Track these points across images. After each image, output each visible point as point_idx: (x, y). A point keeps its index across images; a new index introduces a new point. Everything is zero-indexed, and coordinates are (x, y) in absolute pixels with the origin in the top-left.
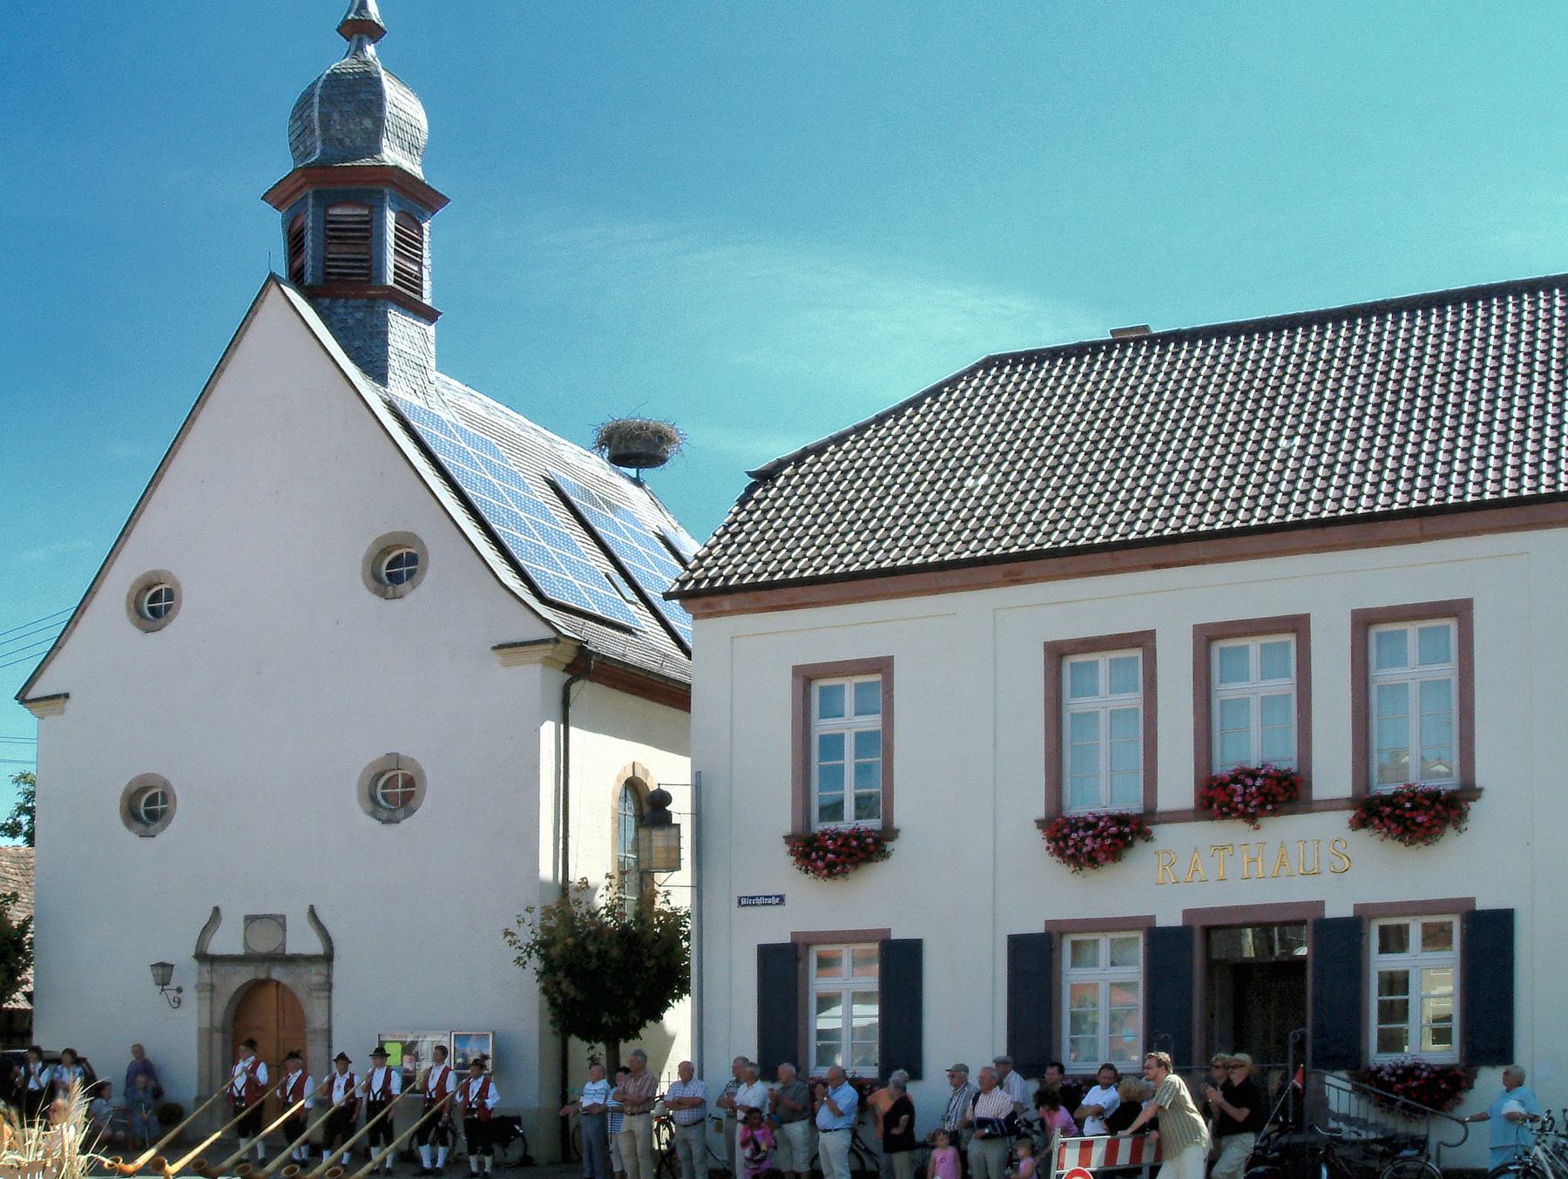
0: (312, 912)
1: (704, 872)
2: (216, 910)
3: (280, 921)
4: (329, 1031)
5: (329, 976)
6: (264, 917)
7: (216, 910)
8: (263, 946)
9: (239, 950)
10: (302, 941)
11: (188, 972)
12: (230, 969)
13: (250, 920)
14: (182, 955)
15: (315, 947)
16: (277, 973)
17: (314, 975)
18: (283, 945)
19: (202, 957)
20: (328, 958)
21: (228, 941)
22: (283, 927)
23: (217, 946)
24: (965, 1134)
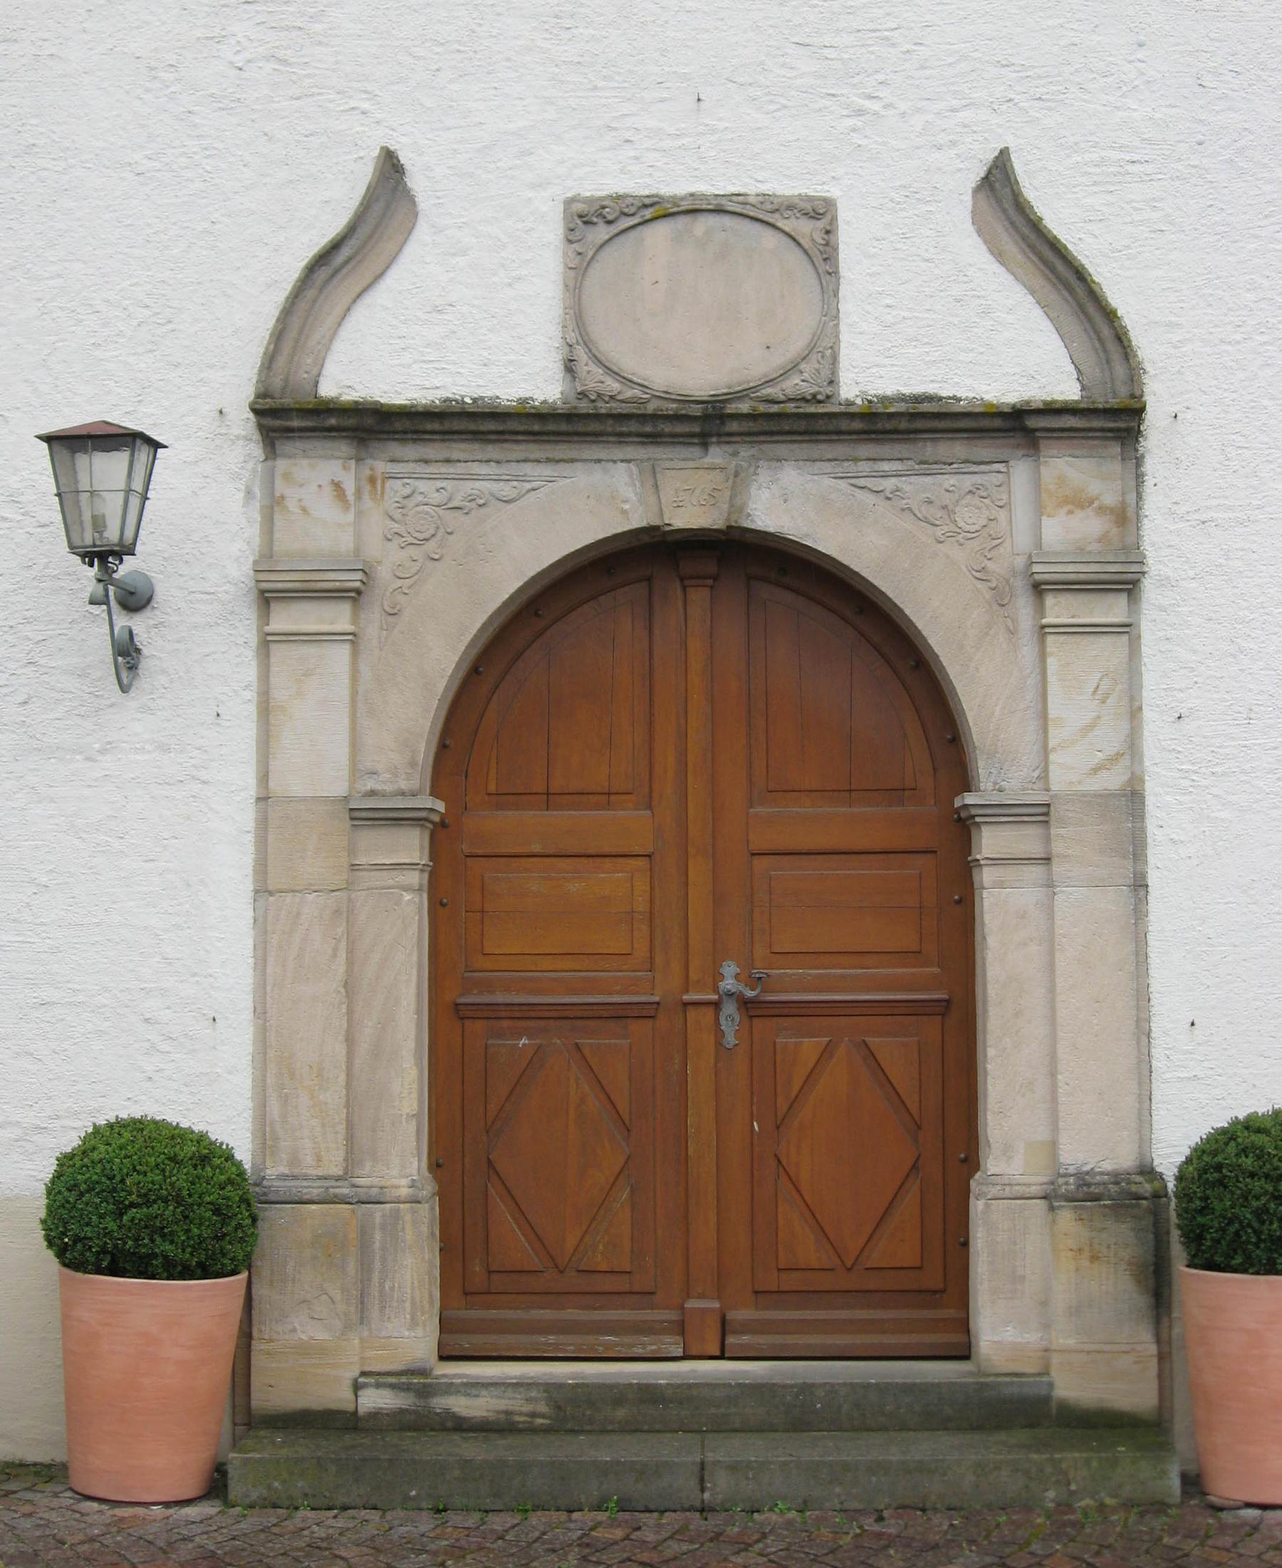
0: (999, 184)
1: (228, 1347)
2: (391, 167)
3: (807, 231)
4: (1133, 798)
5: (1126, 517)
6: (693, 209)
7: (391, 167)
8: (690, 363)
9: (528, 374)
10: (933, 321)
11: (207, 510)
12: (479, 476)
13: (602, 224)
14: (198, 404)
15: (1031, 361)
16: (789, 500)
17: (1045, 512)
18: (824, 346)
19: (290, 418)
20: (1113, 421)
21: (468, 321)
22: (823, 258)
23: (369, 361)
24: (820, 224)
